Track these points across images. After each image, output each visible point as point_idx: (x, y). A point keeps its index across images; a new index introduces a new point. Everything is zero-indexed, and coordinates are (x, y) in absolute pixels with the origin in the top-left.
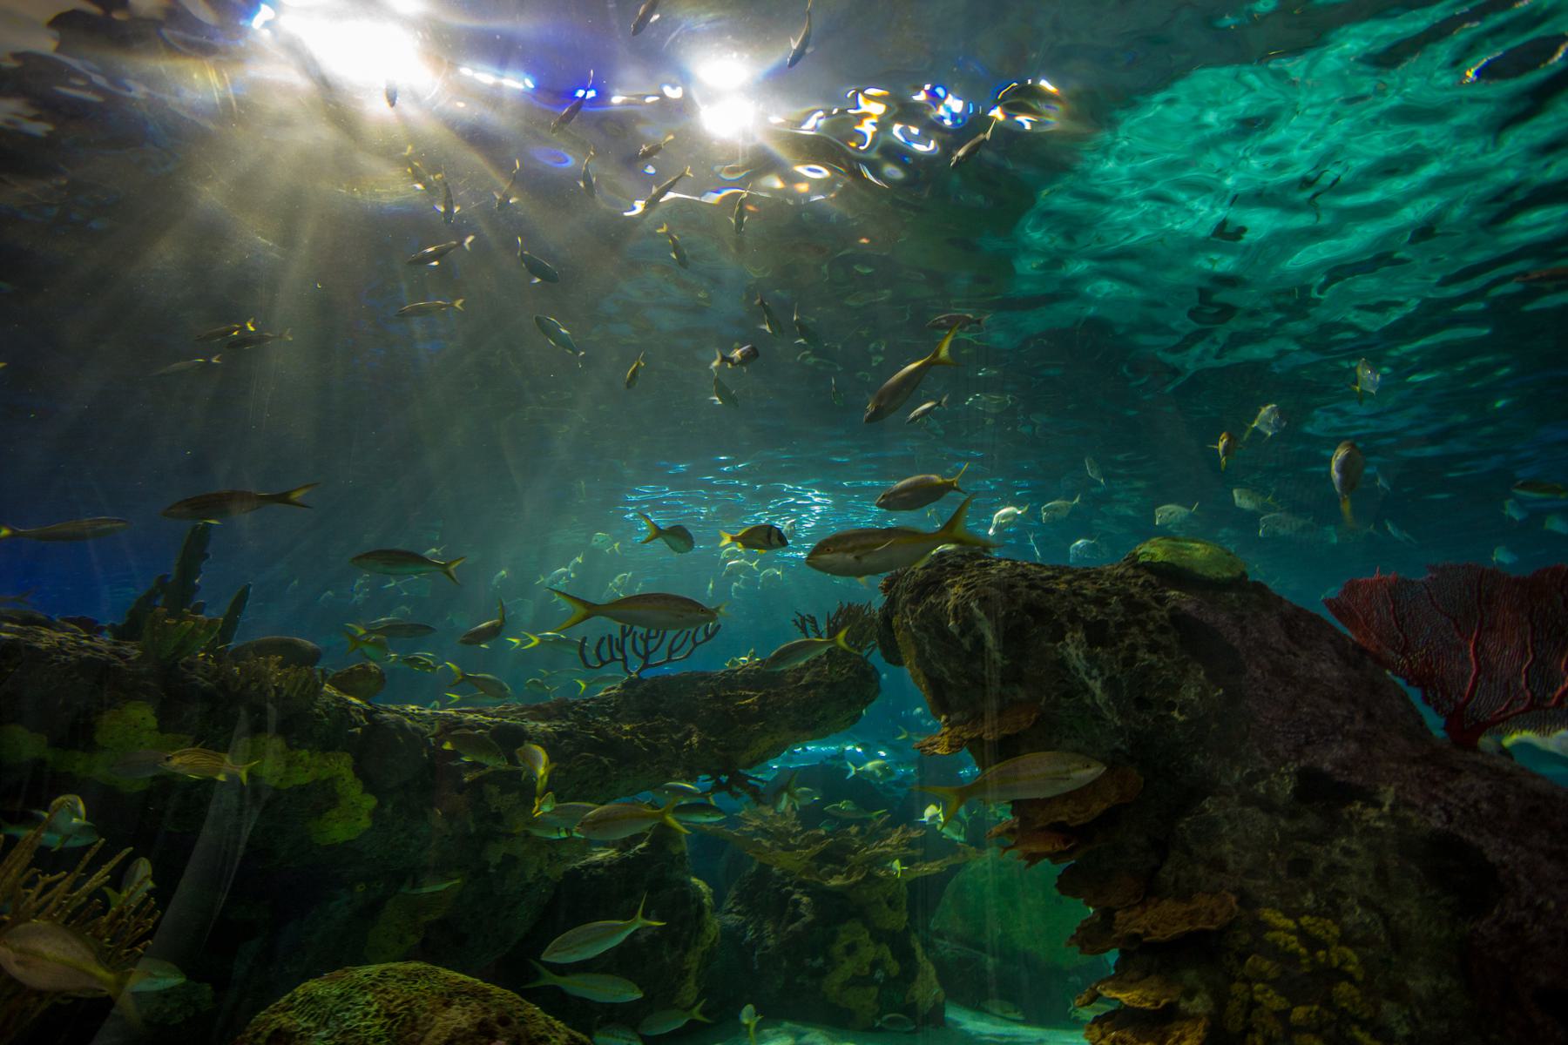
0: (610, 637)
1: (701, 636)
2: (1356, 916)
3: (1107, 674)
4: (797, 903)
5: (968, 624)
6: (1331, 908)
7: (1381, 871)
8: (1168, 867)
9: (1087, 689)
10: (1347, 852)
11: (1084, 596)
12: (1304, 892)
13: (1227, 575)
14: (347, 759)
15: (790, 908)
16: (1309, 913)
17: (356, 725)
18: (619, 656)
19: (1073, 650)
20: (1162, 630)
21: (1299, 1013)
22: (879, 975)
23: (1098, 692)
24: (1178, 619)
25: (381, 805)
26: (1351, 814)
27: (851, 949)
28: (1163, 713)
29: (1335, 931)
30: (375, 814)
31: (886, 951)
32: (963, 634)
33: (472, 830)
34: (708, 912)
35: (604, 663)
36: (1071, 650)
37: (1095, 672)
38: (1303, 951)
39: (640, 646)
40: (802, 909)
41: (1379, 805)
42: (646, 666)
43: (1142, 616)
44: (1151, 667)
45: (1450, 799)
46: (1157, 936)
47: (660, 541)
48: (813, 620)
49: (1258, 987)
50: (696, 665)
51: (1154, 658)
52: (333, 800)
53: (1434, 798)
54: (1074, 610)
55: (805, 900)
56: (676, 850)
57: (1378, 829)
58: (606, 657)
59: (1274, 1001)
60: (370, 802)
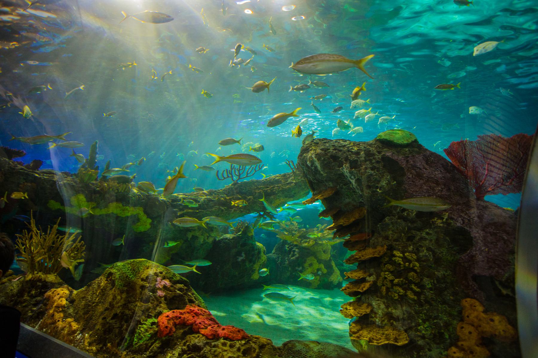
0: (227, 170)
1: (257, 168)
2: (424, 252)
3: (357, 178)
4: (294, 251)
5: (312, 162)
6: (417, 251)
7: (437, 240)
8: (373, 239)
9: (351, 183)
10: (428, 234)
11: (352, 152)
12: (410, 246)
13: (405, 142)
14: (142, 209)
15: (292, 253)
16: (409, 252)
17: (143, 199)
18: (230, 175)
19: (345, 170)
20: (378, 162)
21: (396, 281)
22: (320, 272)
23: (354, 183)
24: (385, 159)
25: (153, 221)
26: (433, 222)
27: (311, 265)
28: (374, 190)
29: (415, 257)
30: (151, 224)
31: (322, 266)
32: (312, 166)
33: (421, 254)
34: (262, 254)
35: (225, 178)
36: (345, 170)
37: (353, 177)
38: (402, 263)
39: (237, 173)
40: (296, 253)
41: (443, 219)
42: (239, 178)
43: (371, 158)
44: (371, 175)
45: (466, 217)
46: (363, 258)
47: (238, 140)
48: (292, 162)
49: (387, 273)
50: (254, 179)
51: (373, 172)
52: (138, 220)
53: (461, 216)
54: (347, 157)
55: (297, 250)
56: (250, 235)
57: (440, 226)
58: (225, 176)
59: (390, 277)
60: (150, 221)
